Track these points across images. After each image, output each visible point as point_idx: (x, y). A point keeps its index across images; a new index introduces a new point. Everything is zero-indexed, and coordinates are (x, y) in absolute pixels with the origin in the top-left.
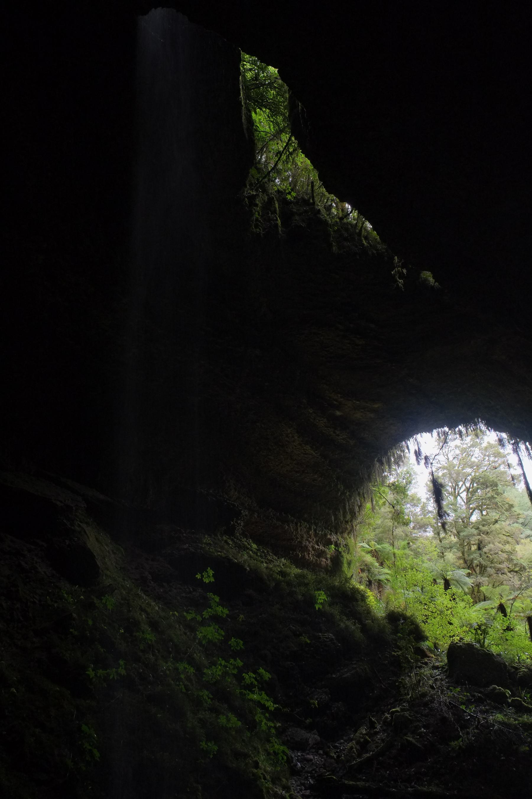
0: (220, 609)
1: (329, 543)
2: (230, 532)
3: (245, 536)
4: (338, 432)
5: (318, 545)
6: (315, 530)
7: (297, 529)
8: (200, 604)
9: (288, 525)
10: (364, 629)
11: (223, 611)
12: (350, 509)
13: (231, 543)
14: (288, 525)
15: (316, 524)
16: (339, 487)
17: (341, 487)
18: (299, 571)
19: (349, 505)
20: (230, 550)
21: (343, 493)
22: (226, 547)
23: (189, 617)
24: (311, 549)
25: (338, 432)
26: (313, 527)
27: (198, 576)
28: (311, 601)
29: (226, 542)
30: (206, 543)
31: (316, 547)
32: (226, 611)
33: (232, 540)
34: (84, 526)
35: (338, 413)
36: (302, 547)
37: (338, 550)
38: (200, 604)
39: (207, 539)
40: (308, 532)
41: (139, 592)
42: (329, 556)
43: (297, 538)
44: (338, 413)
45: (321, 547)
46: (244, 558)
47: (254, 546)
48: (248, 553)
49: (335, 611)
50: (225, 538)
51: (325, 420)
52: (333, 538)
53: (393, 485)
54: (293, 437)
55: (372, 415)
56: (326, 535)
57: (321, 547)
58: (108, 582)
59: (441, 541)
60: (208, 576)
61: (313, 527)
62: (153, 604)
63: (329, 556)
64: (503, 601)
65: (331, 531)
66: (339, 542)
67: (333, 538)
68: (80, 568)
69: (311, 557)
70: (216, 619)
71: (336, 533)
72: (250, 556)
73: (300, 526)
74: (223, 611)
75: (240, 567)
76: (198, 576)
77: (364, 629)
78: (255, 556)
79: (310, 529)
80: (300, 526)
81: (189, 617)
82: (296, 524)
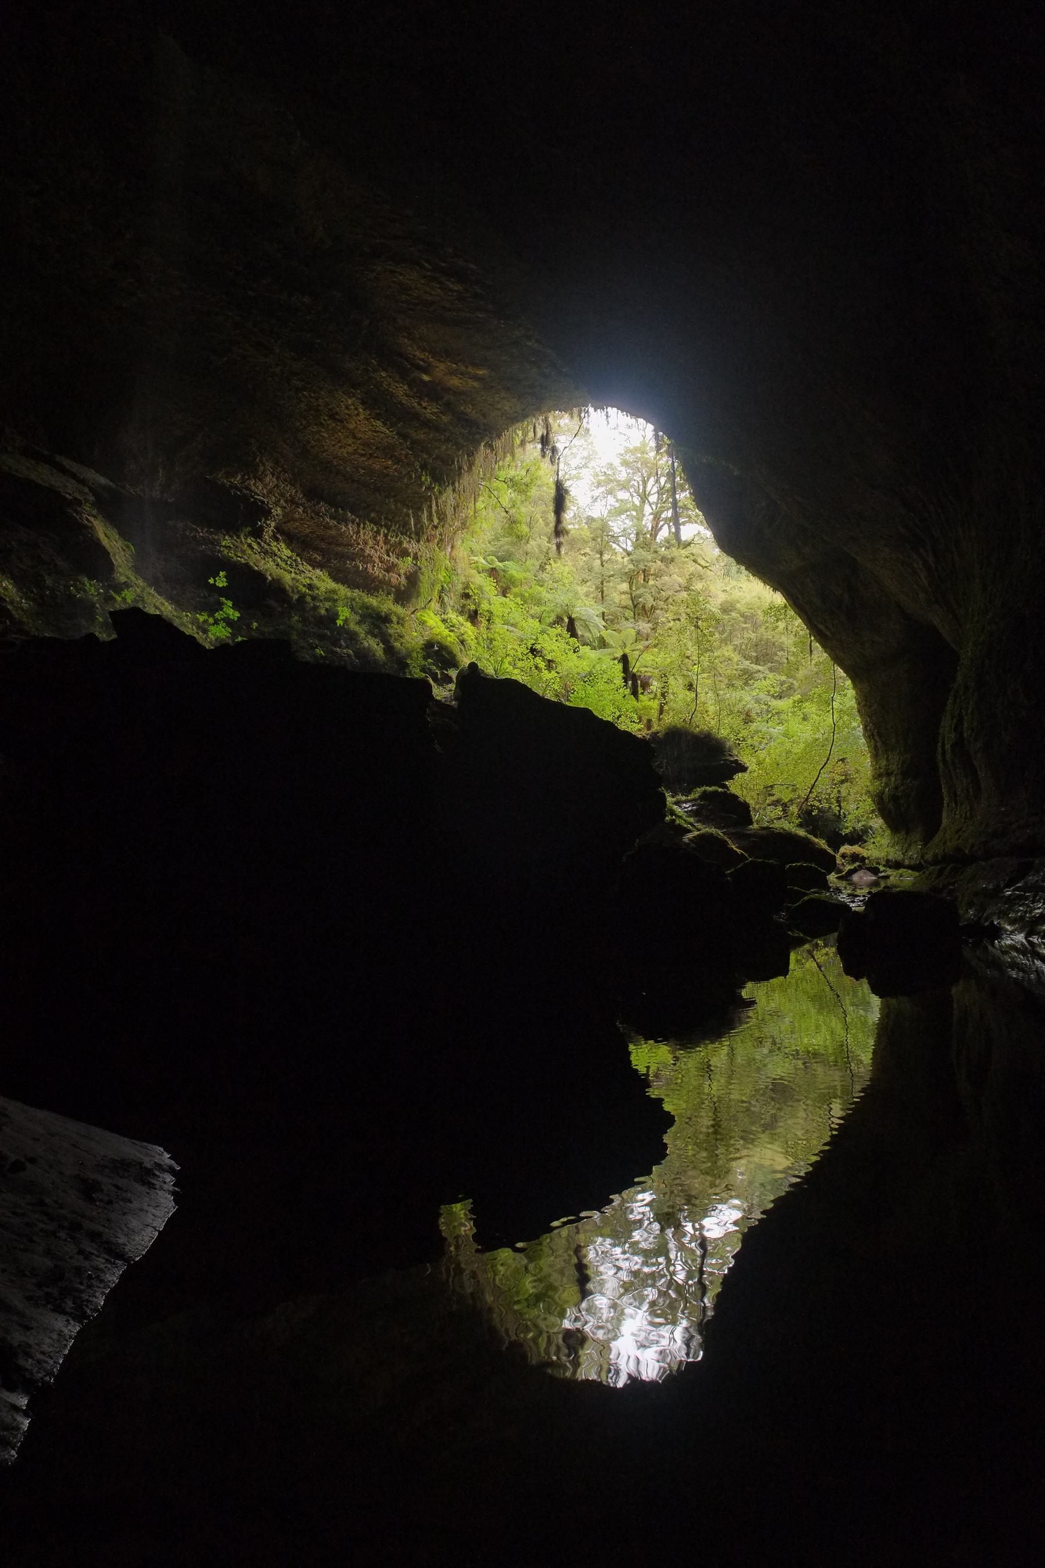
0: (231, 612)
1: (404, 553)
2: (257, 534)
3: (277, 540)
4: (424, 404)
5: (388, 555)
6: (386, 536)
7: (358, 532)
8: (213, 608)
9: (346, 526)
10: (389, 649)
11: (234, 615)
12: (437, 512)
13: (255, 546)
14: (346, 526)
15: (388, 528)
16: (423, 478)
17: (426, 479)
18: (331, 585)
19: (437, 505)
20: (253, 556)
21: (429, 488)
22: (249, 552)
23: (201, 619)
24: (377, 560)
25: (424, 404)
26: (383, 530)
27: (211, 581)
28: (333, 616)
29: (250, 546)
30: (225, 547)
31: (385, 557)
32: (237, 614)
33: (259, 544)
34: (92, 519)
35: (426, 378)
36: (364, 557)
37: (416, 565)
38: (213, 608)
39: (227, 541)
40: (375, 538)
41: (152, 591)
42: (402, 571)
43: (358, 544)
44: (426, 378)
45: (393, 559)
46: (268, 567)
47: (287, 552)
48: (274, 561)
49: (361, 631)
50: (249, 541)
51: (406, 387)
52: (412, 546)
53: (511, 480)
54: (356, 409)
55: (476, 384)
56: (401, 543)
57: (393, 559)
58: (123, 579)
59: (602, 565)
60: (221, 581)
61: (383, 530)
62: (166, 604)
63: (402, 571)
64: (627, 651)
65: (410, 538)
66: (419, 554)
67: (412, 546)
68: (97, 563)
69: (377, 572)
70: (229, 622)
71: (418, 541)
72: (279, 563)
73: (364, 528)
74: (234, 615)
75: (260, 576)
76: (211, 581)
77: (389, 649)
78: (283, 565)
79: (378, 532)
80: (364, 528)
81: (201, 619)
82: (359, 525)
